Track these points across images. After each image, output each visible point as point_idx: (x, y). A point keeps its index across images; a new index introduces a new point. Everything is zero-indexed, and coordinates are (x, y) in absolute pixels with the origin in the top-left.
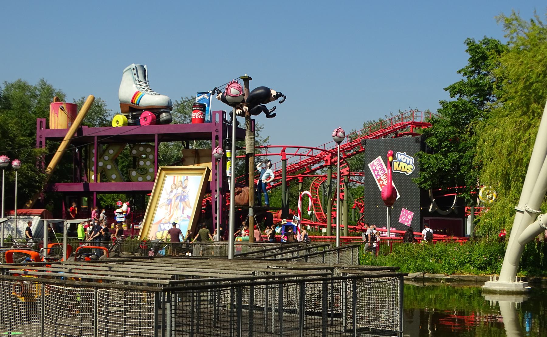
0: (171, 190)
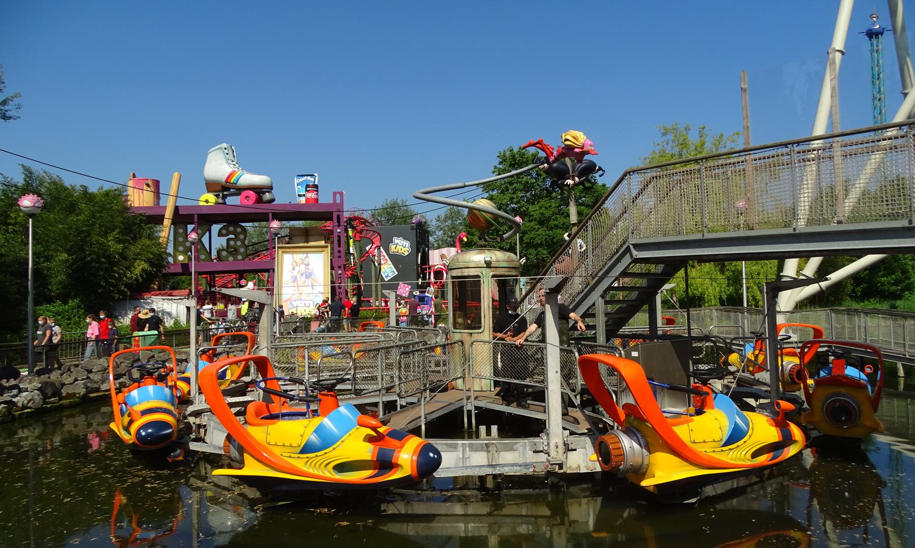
0: (292, 267)
